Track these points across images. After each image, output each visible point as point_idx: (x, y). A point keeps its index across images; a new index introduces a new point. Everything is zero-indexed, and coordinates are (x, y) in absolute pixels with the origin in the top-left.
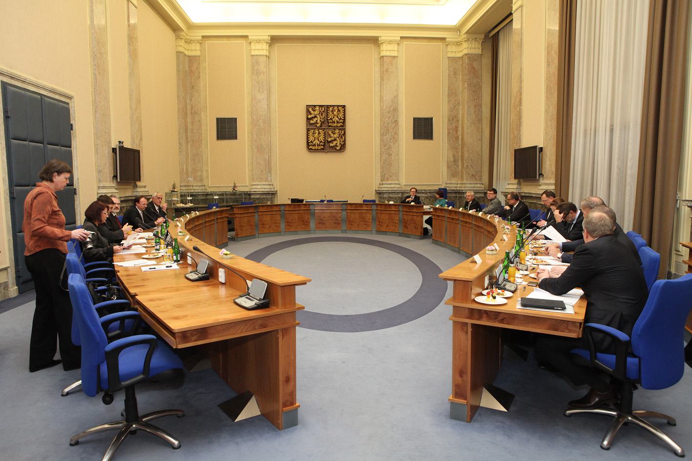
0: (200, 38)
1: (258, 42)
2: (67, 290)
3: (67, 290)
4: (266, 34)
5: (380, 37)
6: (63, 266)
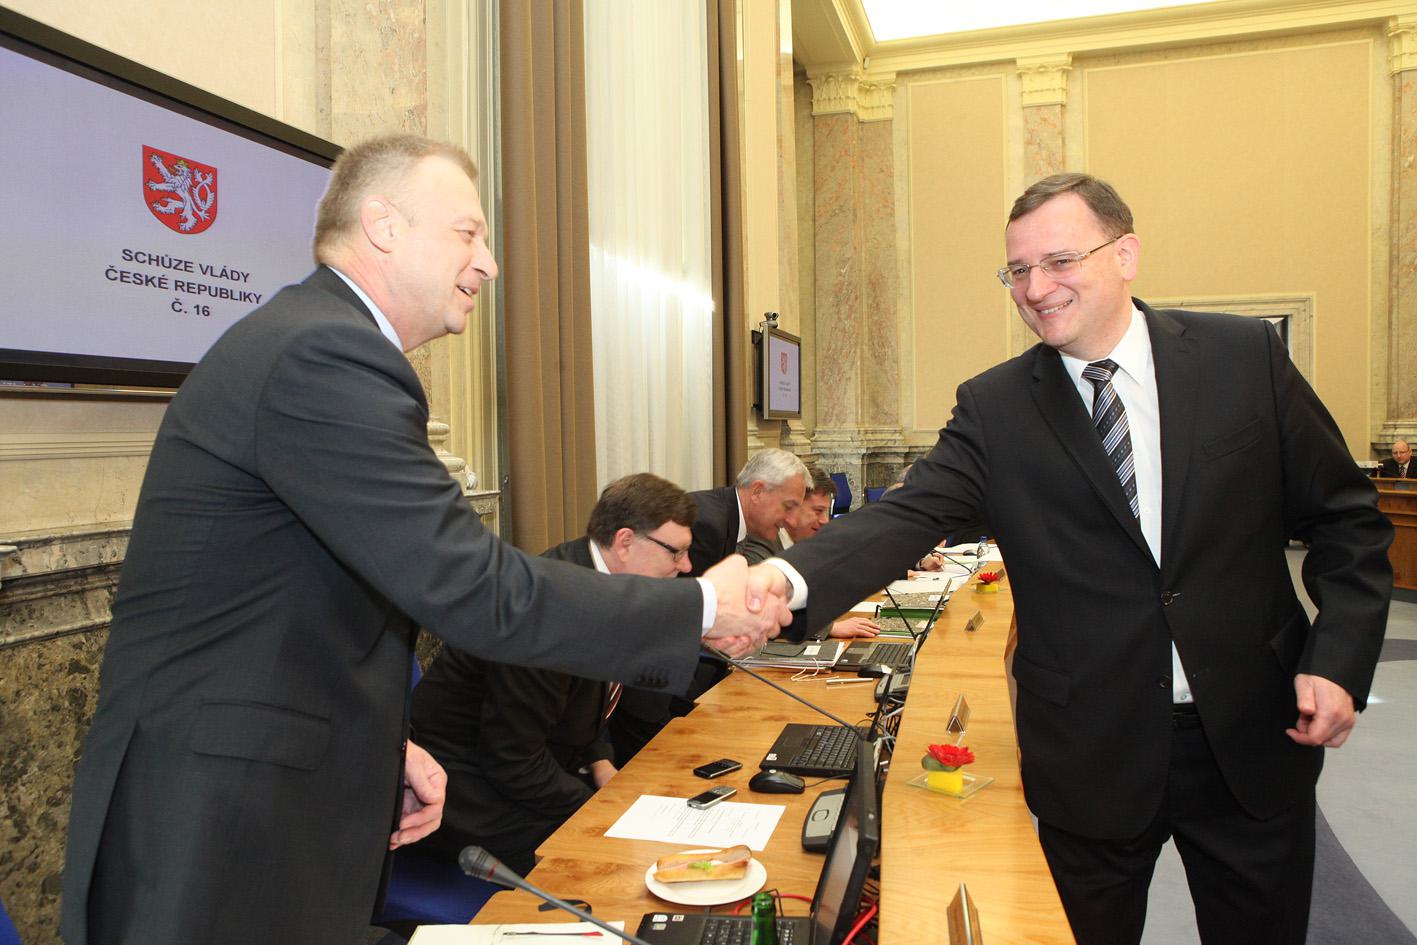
0: (894, 76)
1: (1042, 73)
2: (615, 694)
3: (615, 694)
4: (1061, 49)
5: (1395, 18)
6: (836, 651)
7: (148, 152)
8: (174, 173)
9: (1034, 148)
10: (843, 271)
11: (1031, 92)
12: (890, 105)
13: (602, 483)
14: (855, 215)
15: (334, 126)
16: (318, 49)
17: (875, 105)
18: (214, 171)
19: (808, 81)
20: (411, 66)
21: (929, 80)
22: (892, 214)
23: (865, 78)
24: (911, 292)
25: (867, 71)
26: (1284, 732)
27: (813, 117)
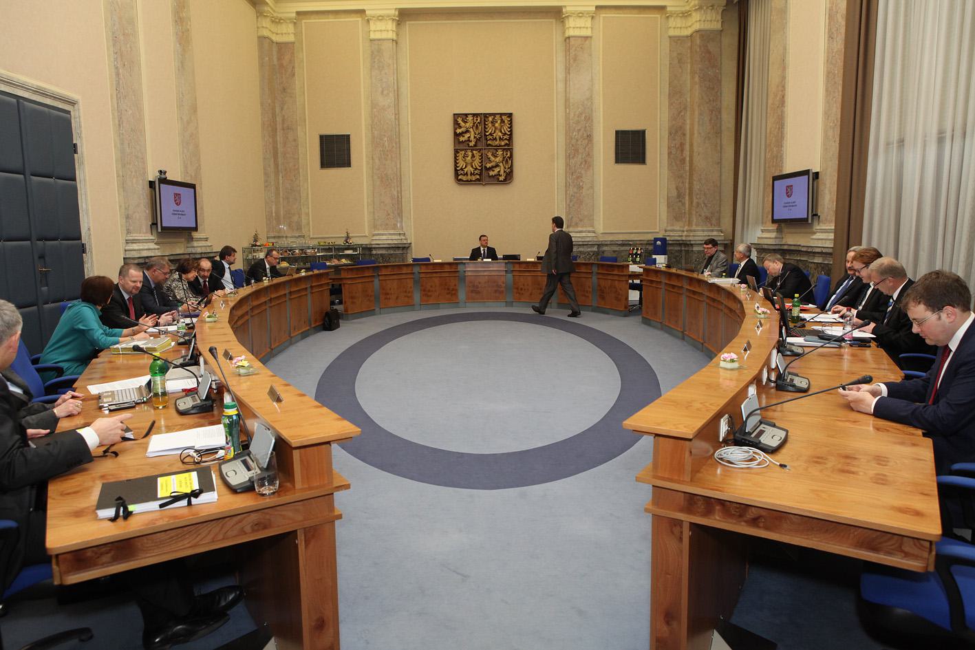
0: (594, 9)
1: (580, 17)
11: (375, 31)
13: (86, 277)
17: (284, 32)
26: (952, 530)
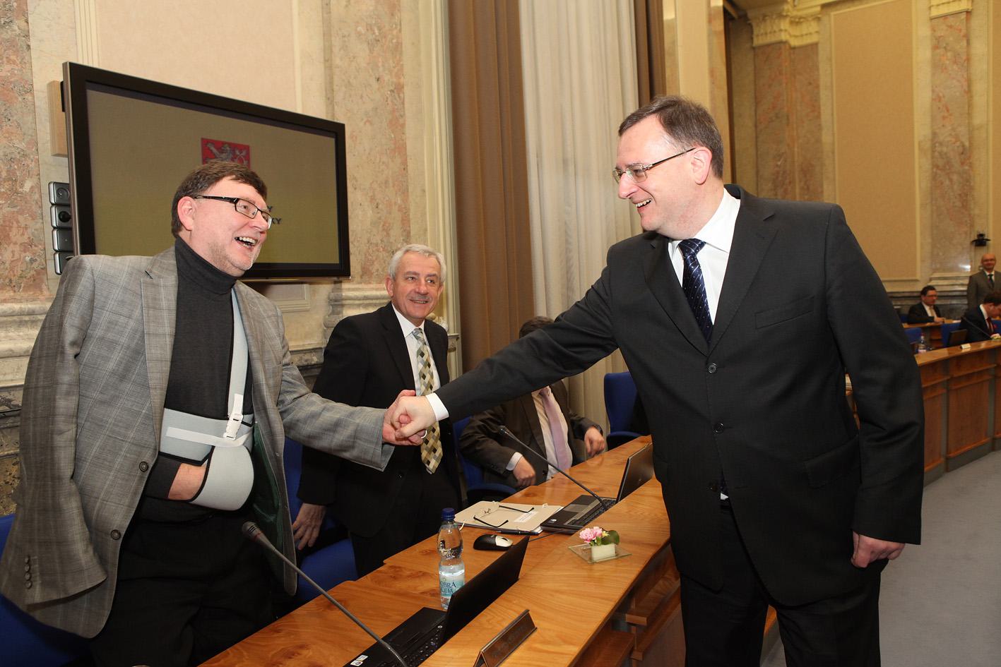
0: (819, 9)
7: (205, 142)
8: (222, 152)
9: (941, 51)
10: (779, 163)
12: (817, 32)
14: (788, 119)
15: (336, 107)
16: (326, 61)
17: (804, 33)
18: (247, 148)
19: (749, 22)
20: (391, 61)
21: (849, 7)
22: (819, 117)
23: (795, 13)
24: (834, 168)
25: (798, 8)
27: (754, 48)
